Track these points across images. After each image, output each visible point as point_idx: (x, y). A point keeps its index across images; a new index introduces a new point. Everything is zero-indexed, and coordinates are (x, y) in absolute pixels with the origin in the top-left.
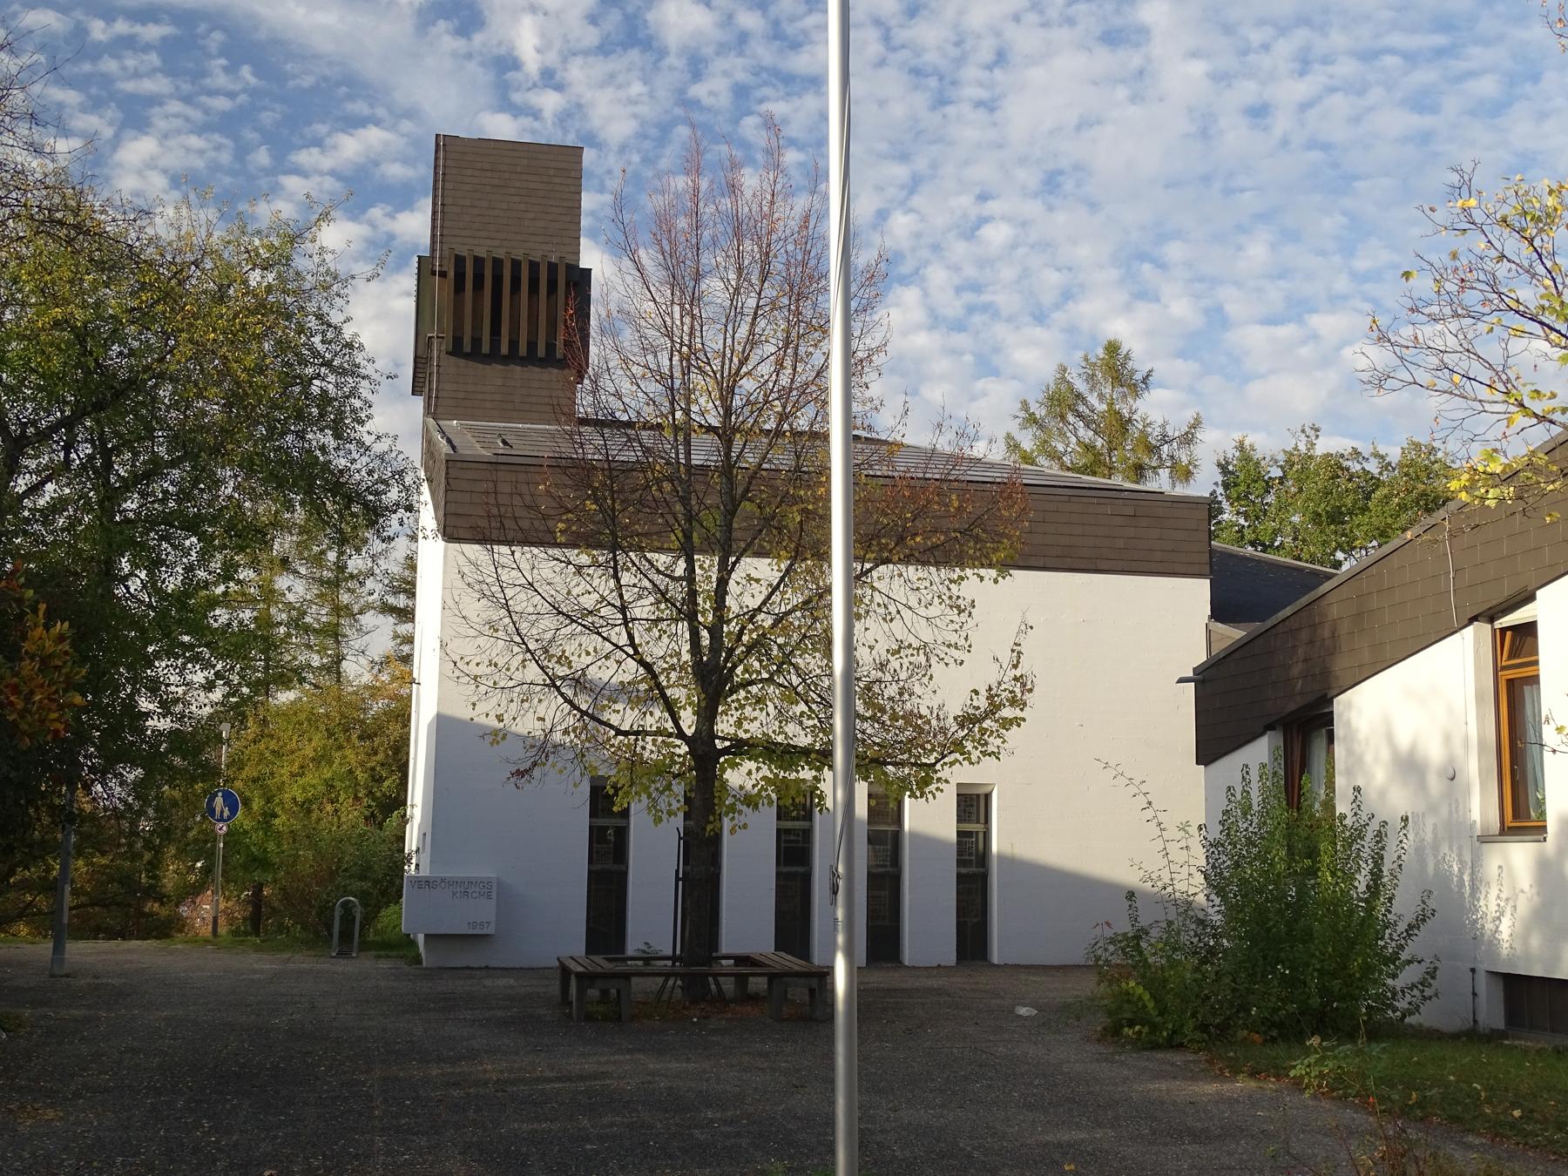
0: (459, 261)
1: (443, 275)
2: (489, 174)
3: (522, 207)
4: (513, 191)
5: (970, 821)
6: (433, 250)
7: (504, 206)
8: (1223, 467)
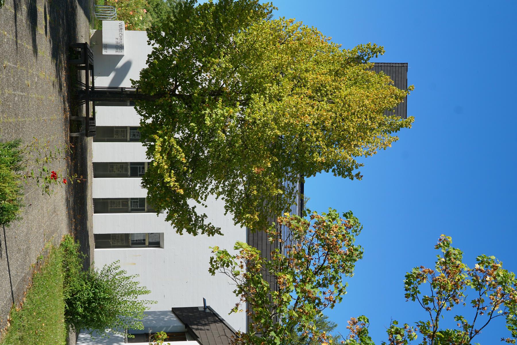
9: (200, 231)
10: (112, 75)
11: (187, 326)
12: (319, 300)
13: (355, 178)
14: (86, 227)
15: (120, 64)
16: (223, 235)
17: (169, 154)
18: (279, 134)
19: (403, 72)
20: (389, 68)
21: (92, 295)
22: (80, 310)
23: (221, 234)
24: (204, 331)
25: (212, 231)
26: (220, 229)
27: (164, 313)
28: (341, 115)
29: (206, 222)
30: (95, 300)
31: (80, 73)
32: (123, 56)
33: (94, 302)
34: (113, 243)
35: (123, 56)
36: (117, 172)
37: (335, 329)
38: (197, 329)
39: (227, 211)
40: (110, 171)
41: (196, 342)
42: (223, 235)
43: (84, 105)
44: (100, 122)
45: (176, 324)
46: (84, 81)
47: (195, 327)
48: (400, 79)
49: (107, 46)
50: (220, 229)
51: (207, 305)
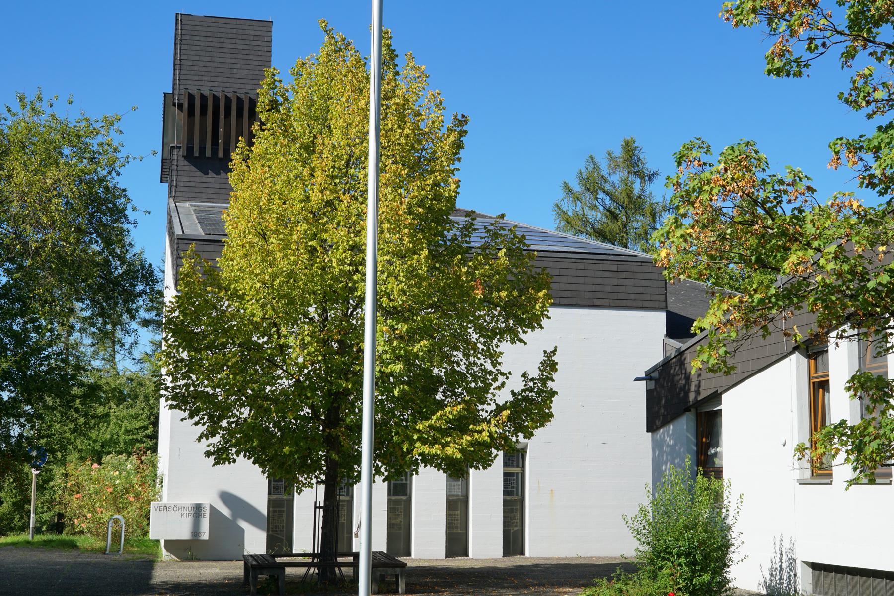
0: (191, 98)
1: (180, 106)
2: (211, 39)
3: (233, 61)
4: (226, 50)
5: (512, 466)
6: (174, 89)
7: (221, 60)
8: (221, 456)
9: (550, 384)
10: (243, 524)
11: (688, 410)
12: (795, 208)
13: (465, 128)
14: (510, 569)
15: (225, 511)
16: (556, 347)
17: (446, 432)
18: (425, 252)
19: (193, 23)
20: (184, 47)
21: (682, 560)
22: (706, 577)
23: (555, 350)
24: (703, 383)
25: (549, 365)
26: (545, 352)
27: (657, 445)
28: (785, 192)
29: (534, 373)
30: (690, 554)
31: (289, 576)
32: (211, 507)
33: (695, 556)
34: (516, 526)
35: (211, 507)
36: (401, 518)
37: (598, 159)
38: (698, 392)
39: (521, 340)
40: (400, 529)
41: (724, 396)
42: (556, 347)
43: (289, 570)
44: (380, 545)
45: (681, 430)
46: (302, 571)
47: (692, 396)
48: (204, 29)
49: (196, 532)
50: (545, 352)
51: (643, 376)
